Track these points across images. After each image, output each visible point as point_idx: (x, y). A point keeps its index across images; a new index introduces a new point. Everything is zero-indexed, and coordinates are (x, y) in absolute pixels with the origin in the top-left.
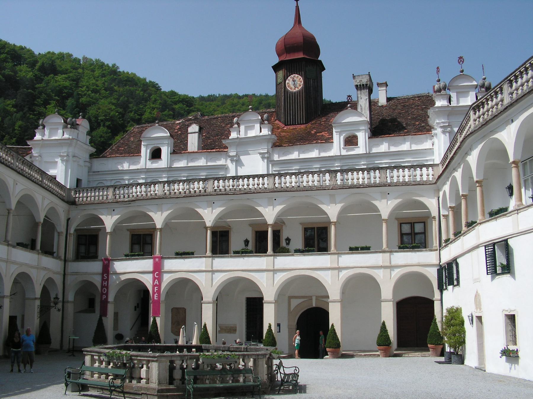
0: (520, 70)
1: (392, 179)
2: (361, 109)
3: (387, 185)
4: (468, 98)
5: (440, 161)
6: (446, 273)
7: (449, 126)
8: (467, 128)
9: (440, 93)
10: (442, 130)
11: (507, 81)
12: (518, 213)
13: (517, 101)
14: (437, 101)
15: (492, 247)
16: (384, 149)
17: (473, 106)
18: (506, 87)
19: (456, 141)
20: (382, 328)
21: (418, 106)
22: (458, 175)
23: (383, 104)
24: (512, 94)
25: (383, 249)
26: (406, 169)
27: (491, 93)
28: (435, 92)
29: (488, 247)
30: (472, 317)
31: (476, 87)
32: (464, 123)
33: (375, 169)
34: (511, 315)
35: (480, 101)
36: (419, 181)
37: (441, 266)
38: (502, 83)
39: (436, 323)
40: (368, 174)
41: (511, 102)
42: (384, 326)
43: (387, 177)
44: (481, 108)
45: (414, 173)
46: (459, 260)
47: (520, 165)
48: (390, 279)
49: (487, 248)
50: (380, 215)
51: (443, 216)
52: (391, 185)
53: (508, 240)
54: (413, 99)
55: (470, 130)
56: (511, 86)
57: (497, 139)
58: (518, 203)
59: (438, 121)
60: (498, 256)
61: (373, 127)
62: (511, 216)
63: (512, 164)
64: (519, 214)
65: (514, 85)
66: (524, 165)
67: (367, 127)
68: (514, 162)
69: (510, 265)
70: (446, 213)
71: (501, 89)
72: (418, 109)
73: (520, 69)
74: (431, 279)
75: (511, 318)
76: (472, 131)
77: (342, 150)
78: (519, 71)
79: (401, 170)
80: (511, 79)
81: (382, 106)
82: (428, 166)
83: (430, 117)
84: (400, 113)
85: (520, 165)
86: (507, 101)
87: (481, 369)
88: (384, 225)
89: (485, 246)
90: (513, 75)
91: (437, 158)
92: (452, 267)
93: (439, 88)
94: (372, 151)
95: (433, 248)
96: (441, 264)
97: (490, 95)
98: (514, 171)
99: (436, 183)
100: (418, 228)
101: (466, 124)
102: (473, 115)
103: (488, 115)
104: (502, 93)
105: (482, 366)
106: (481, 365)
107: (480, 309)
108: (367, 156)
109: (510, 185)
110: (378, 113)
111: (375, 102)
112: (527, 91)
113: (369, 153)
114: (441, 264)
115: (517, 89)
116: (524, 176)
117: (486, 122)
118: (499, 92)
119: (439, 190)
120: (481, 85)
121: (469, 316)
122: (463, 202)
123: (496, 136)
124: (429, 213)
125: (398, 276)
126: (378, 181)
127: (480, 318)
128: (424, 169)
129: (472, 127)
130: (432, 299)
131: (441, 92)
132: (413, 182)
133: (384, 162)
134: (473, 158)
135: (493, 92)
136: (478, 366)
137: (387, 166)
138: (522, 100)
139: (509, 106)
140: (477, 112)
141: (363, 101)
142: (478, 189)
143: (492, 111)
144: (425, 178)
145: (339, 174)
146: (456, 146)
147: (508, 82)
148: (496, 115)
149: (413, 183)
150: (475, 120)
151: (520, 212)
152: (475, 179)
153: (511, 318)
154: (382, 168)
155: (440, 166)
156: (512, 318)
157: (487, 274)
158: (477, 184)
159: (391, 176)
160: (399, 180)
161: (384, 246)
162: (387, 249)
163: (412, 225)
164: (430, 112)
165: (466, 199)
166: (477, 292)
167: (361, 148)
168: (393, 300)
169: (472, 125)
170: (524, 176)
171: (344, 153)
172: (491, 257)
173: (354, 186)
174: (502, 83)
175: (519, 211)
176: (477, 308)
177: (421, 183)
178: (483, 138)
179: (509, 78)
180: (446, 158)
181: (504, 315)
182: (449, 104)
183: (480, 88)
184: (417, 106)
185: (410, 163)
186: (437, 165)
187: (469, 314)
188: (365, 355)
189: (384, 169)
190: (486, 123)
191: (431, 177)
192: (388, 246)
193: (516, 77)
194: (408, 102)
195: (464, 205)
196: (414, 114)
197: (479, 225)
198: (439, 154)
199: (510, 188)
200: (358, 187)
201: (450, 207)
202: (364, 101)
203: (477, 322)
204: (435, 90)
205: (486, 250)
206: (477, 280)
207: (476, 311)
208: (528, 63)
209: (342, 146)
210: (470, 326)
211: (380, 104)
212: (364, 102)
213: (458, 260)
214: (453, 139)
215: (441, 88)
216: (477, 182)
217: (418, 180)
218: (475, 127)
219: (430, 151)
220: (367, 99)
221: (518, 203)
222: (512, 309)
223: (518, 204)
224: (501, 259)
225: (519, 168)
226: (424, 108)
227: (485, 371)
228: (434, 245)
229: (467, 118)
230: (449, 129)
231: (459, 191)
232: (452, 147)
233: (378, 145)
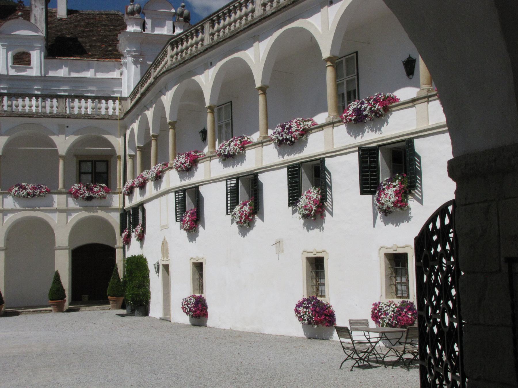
0: (224, 11)
1: (72, 111)
2: (36, 20)
3: (67, 117)
4: (164, 29)
5: (129, 95)
6: (130, 219)
7: (141, 55)
8: (163, 63)
9: (134, 16)
10: (133, 60)
11: (209, 20)
12: (210, 160)
13: (218, 44)
14: (130, 26)
15: (183, 193)
16: (63, 74)
17: (172, 41)
18: (207, 26)
19: (149, 76)
20: (55, 278)
21: (105, 25)
22: (150, 113)
23: (62, 17)
24: (212, 34)
25: (59, 189)
26: (90, 100)
27: (191, 30)
28: (127, 14)
29: (178, 193)
30: (158, 266)
31: (174, 14)
32: (160, 57)
33: (52, 97)
34: (199, 263)
35: (180, 36)
36: (104, 115)
37: (124, 210)
38: (204, 22)
39: (117, 272)
40: (43, 101)
41: (211, 44)
42: (57, 277)
43: (66, 107)
44: (179, 44)
45: (99, 105)
46: (146, 206)
47: (216, 110)
48: (67, 223)
49: (177, 194)
50: (56, 151)
51: (130, 156)
52: (71, 117)
53: (200, 187)
54: (100, 17)
55: (166, 66)
56: (213, 27)
57: (194, 80)
58: (211, 150)
59: (128, 49)
60: (188, 202)
61: (50, 44)
62: (203, 162)
63: (208, 109)
64: (212, 161)
65: (216, 25)
66: (220, 110)
67: (42, 44)
68: (209, 107)
69: (200, 210)
70: (133, 153)
71: (203, 28)
72: (105, 29)
73: (223, 10)
74: (113, 224)
75: (199, 267)
76: (168, 68)
77: (10, 68)
78: (222, 12)
79: (83, 101)
80: (214, 19)
81: (61, 20)
82: (114, 99)
83: (120, 42)
84: (83, 32)
85: (216, 110)
86: (208, 41)
87: (166, 319)
88: (61, 163)
89: (175, 192)
90: (216, 15)
91: (126, 91)
92: (138, 213)
93: (132, 10)
94: (48, 74)
95: (116, 190)
96: (125, 208)
97: (190, 32)
98: (209, 117)
99: (122, 119)
100: (101, 167)
101: (163, 58)
102: (170, 51)
103: (186, 53)
104: (203, 33)
105: (168, 317)
106: (166, 316)
107: (167, 257)
108: (42, 79)
109: (204, 129)
110: (56, 27)
111: (52, 13)
112: (229, 35)
113: (45, 76)
114: (125, 208)
115: (219, 31)
116: (218, 122)
117: (185, 61)
118: (200, 31)
119: (126, 127)
120: (179, 14)
121: (155, 265)
122: (153, 143)
123: (193, 78)
124: (114, 151)
125: (76, 220)
126: (55, 110)
127: (166, 267)
128: (110, 102)
129: (169, 63)
130: (113, 247)
131: (135, 16)
132: (97, 115)
133: (64, 90)
134: (167, 99)
135: (194, 29)
136: (163, 316)
137: (67, 94)
138: (223, 44)
139: (209, 48)
140: (175, 48)
141: (38, 10)
142: (171, 132)
143: (191, 50)
144: (111, 112)
145: (5, 98)
146: (149, 81)
147: (210, 21)
148: (195, 56)
149: (97, 117)
150: (172, 57)
151: (213, 159)
152: (168, 120)
153: (199, 267)
154: (61, 97)
155: (129, 100)
156: (199, 267)
157: (176, 221)
158: (170, 126)
159: (71, 106)
160: (80, 112)
161: (61, 186)
162: (64, 190)
163: (94, 163)
164: (121, 37)
165: (156, 140)
166: (164, 239)
167: (35, 69)
168: (69, 247)
169: (168, 61)
170: (218, 122)
171: (12, 72)
172: (181, 205)
173: (25, 114)
174: (204, 22)
175: (212, 158)
176: (163, 257)
177: (106, 118)
178: (179, 79)
179: (212, 17)
180: (136, 92)
181: (192, 264)
182: (143, 31)
183: (178, 17)
184: (104, 25)
185: (93, 93)
186: (125, 99)
187: (155, 262)
188: (34, 311)
189: (64, 98)
190: (184, 62)
191: (117, 112)
192: (64, 186)
193: (219, 18)
194: (93, 19)
195: (154, 146)
196: (100, 35)
197: (170, 170)
198: (129, 87)
199: (204, 133)
200: (30, 115)
201: (138, 147)
202: (39, 10)
203: (163, 270)
204: (128, 11)
205: (176, 196)
206: (164, 227)
207: (163, 260)
208: (232, 5)
209: (10, 64)
210: (156, 275)
211: (58, 17)
212: (39, 12)
213: (144, 205)
214: (146, 73)
215: (135, 10)
216: (170, 123)
217: (103, 113)
218: (172, 65)
219: (118, 82)
220: (43, 8)
221: (211, 150)
222: (200, 257)
223: (211, 150)
224: (190, 206)
225: (215, 114)
226: (112, 29)
227: (170, 321)
228: (118, 187)
229: (163, 53)
230: (141, 59)
231: (149, 130)
232: (144, 81)
233: (57, 68)
